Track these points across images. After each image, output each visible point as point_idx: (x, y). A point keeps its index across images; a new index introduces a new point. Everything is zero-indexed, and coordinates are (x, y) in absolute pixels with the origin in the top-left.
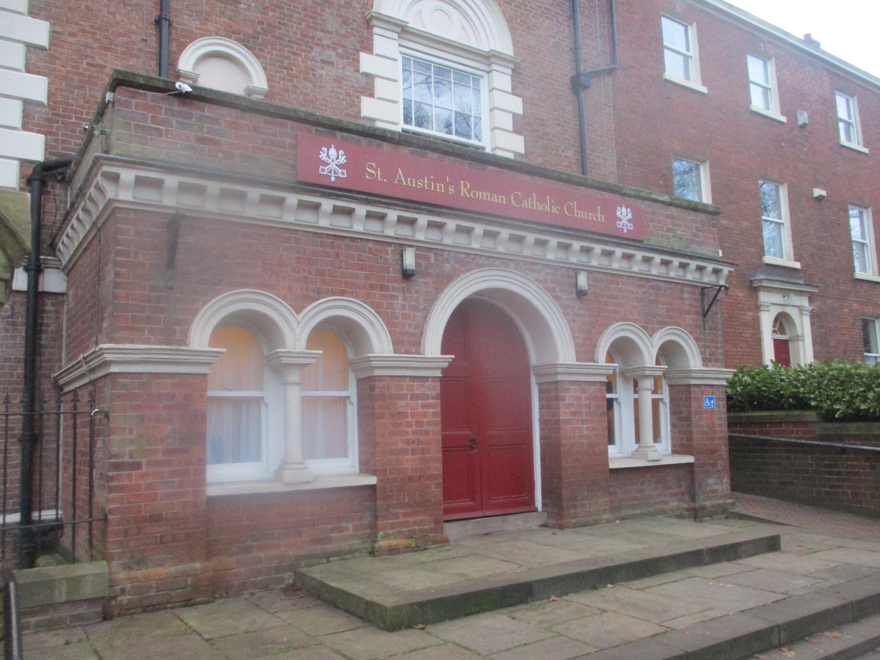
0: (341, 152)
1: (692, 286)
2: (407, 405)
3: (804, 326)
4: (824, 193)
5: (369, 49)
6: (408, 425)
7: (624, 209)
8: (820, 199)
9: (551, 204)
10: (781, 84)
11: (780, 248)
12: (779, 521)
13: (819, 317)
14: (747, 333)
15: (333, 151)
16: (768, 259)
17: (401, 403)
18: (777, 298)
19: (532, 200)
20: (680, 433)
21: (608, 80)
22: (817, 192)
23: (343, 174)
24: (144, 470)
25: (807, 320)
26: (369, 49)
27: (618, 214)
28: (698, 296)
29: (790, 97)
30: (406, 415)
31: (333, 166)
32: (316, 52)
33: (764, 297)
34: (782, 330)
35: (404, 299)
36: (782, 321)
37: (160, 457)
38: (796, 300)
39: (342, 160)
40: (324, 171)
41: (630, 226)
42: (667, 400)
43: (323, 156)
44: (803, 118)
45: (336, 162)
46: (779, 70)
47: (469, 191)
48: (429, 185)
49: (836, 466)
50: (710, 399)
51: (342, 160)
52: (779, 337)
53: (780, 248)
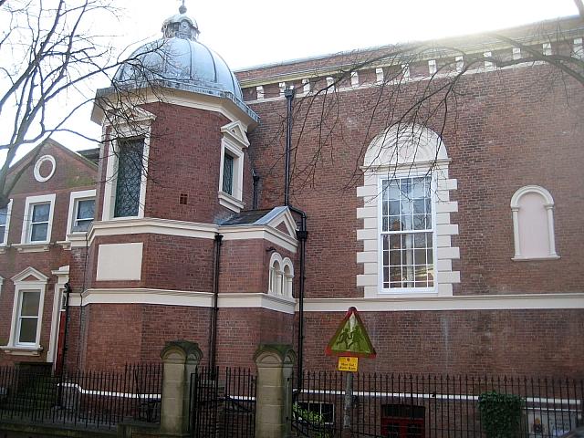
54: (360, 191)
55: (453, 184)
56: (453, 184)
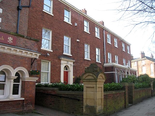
0: (12, 38)
1: (29, 58)
3: (71, 69)
4: (79, 41)
7: (10, 38)
8: (78, 42)
10: (72, 17)
11: (67, 51)
12: (41, 114)
13: (75, 67)
14: (57, 69)
16: (64, 53)
18: (66, 62)
20: (22, 92)
22: (78, 40)
23: (12, 42)
25: (72, 67)
28: (31, 60)
29: (73, 20)
31: (10, 40)
33: (62, 62)
34: (67, 69)
36: (66, 67)
38: (70, 63)
40: (8, 41)
41: (12, 42)
42: (21, 85)
43: (9, 39)
44: (76, 24)
45: (11, 40)
46: (72, 14)
49: (59, 101)
52: (66, 71)
53: (67, 51)
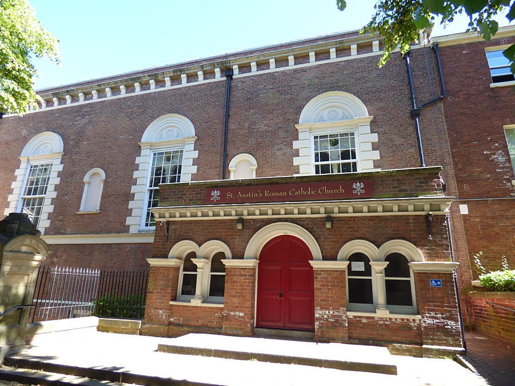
2: (238, 278)
5: (297, 139)
6: (237, 286)
9: (311, 190)
15: (358, 184)
17: (236, 277)
19: (300, 191)
21: (441, 105)
24: (232, 322)
26: (297, 139)
27: (212, 194)
30: (237, 282)
32: (276, 147)
35: (240, 239)
37: (159, 290)
39: (362, 186)
43: (354, 187)
47: (269, 194)
48: (251, 195)
50: (436, 282)
51: (362, 186)
54: (296, 145)
55: (375, 138)
56: (375, 138)
